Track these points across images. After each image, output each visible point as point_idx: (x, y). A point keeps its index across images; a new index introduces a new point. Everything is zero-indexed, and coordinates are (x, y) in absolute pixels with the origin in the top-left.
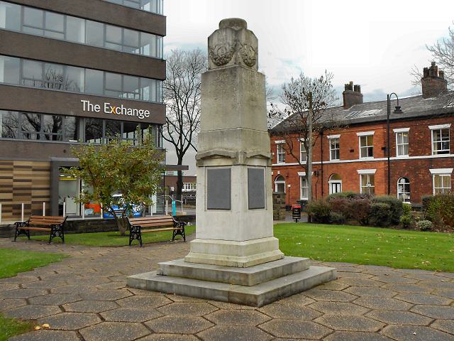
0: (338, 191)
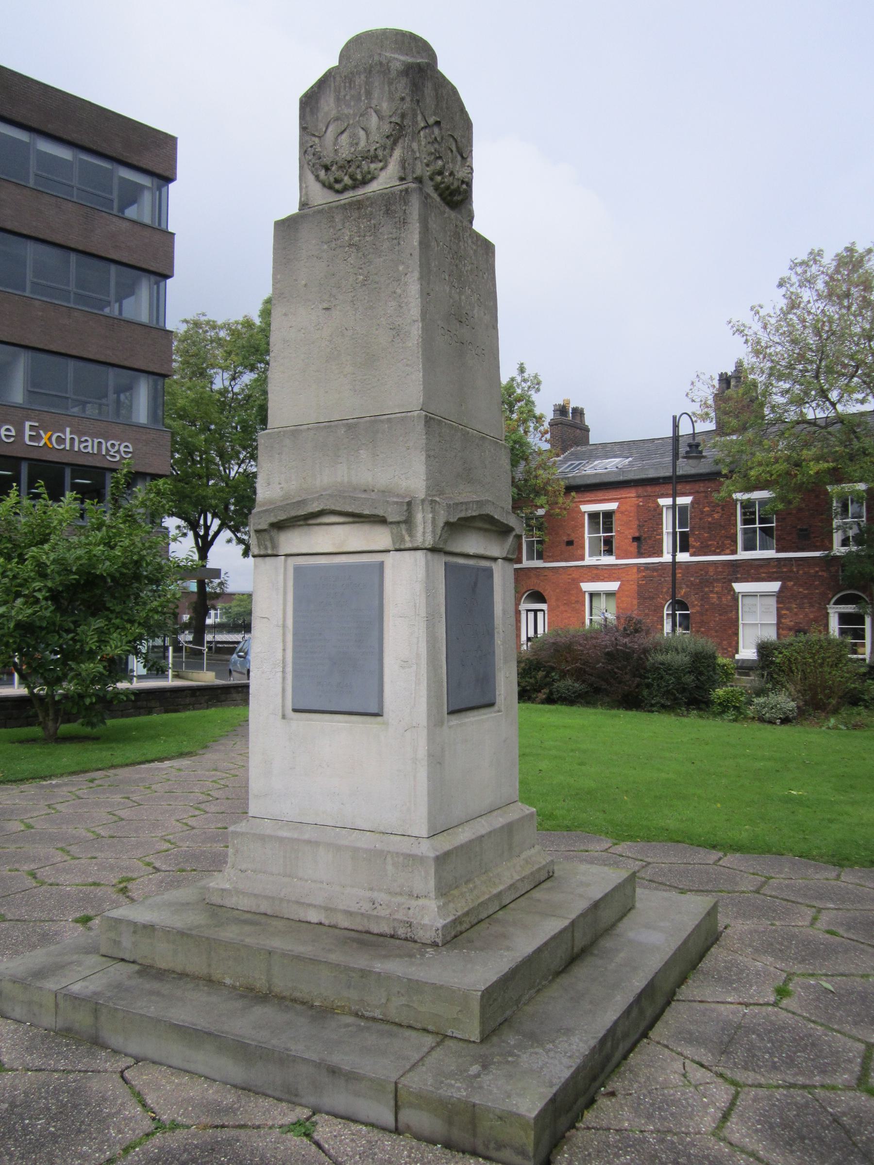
0: (540, 631)
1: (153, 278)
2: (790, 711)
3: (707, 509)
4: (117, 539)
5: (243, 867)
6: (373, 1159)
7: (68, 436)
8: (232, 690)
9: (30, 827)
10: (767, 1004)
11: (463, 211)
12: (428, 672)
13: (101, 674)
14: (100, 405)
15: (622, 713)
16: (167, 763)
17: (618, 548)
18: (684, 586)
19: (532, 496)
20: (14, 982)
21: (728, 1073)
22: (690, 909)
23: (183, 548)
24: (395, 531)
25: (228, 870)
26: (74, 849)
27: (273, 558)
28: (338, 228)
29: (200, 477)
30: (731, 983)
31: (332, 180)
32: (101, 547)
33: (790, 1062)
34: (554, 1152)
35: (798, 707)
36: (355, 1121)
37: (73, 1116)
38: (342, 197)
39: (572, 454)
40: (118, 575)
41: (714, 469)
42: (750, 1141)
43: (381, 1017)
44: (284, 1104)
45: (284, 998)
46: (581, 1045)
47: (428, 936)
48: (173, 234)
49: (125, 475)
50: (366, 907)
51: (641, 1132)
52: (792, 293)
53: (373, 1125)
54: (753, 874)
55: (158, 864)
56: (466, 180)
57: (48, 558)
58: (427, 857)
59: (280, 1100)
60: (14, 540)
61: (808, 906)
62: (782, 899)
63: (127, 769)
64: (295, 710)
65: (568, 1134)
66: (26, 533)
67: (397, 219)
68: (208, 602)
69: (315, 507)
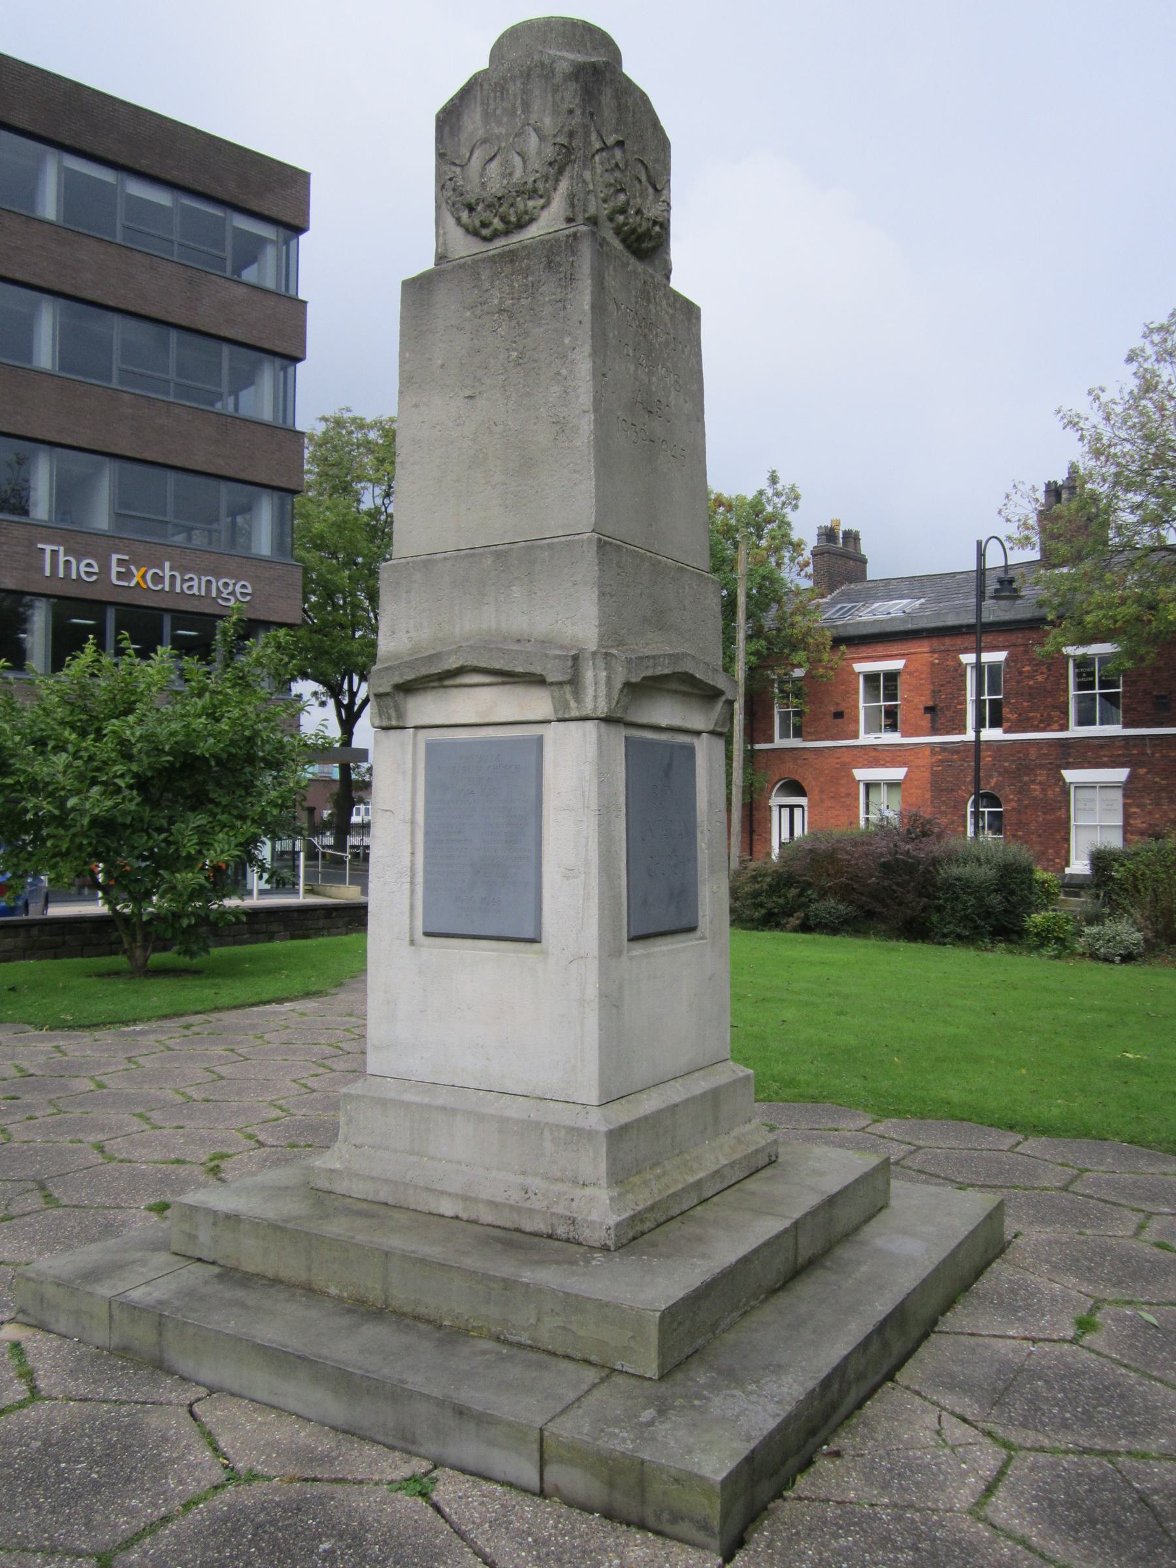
0: (798, 832)
1: (278, 362)
2: (1134, 945)
3: (1027, 668)
4: (225, 709)
5: (359, 1141)
6: (507, 1528)
7: (168, 573)
9: (101, 1086)
10: (1063, 1340)
11: (657, 262)
12: (599, 885)
13: (202, 887)
14: (210, 531)
15: (902, 945)
16: (288, 1006)
17: (904, 722)
18: (995, 774)
19: (786, 651)
20: (59, 1285)
21: (999, 1431)
22: (965, 1210)
23: (318, 719)
24: (556, 694)
25: (339, 1146)
26: (156, 1116)
27: (398, 731)
28: (485, 288)
29: (343, 627)
30: (1015, 1310)
31: (477, 223)
32: (203, 720)
33: (1088, 1420)
34: (751, 1527)
35: (1146, 940)
36: (488, 1479)
37: (122, 1458)
38: (491, 246)
39: (843, 594)
40: (224, 756)
41: (1037, 613)
42: (1020, 1524)
43: (529, 1342)
44: (397, 1453)
45: (404, 1314)
46: (795, 1386)
47: (596, 1235)
48: (305, 303)
49: (234, 624)
50: (516, 1197)
51: (872, 1505)
52: (1146, 370)
53: (511, 1485)
54: (1062, 1165)
55: (262, 1137)
56: (660, 219)
57: (133, 734)
58: (597, 1132)
59: (392, 1448)
60: (90, 710)
61: (1133, 1210)
62: (1099, 1199)
63: (234, 1013)
64: (427, 934)
65: (771, 1505)
66: (105, 701)
67: (562, 275)
68: (354, 794)
69: (453, 663)
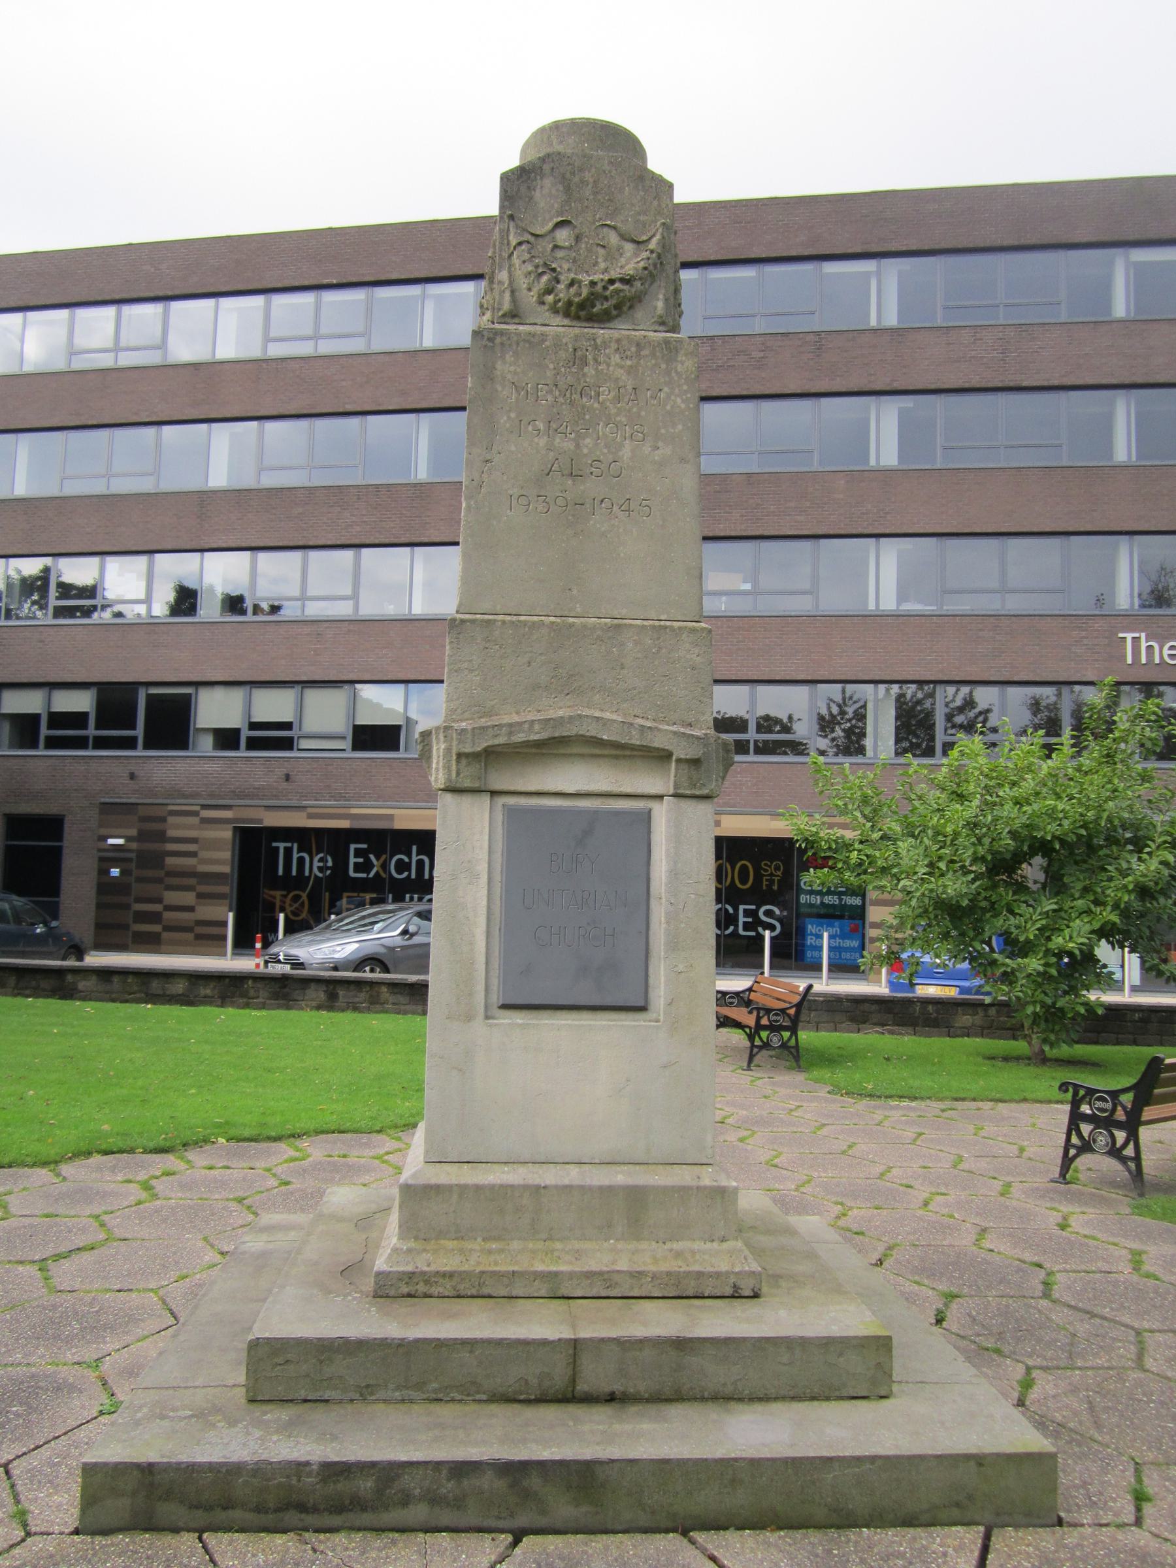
8: (836, 1465)
